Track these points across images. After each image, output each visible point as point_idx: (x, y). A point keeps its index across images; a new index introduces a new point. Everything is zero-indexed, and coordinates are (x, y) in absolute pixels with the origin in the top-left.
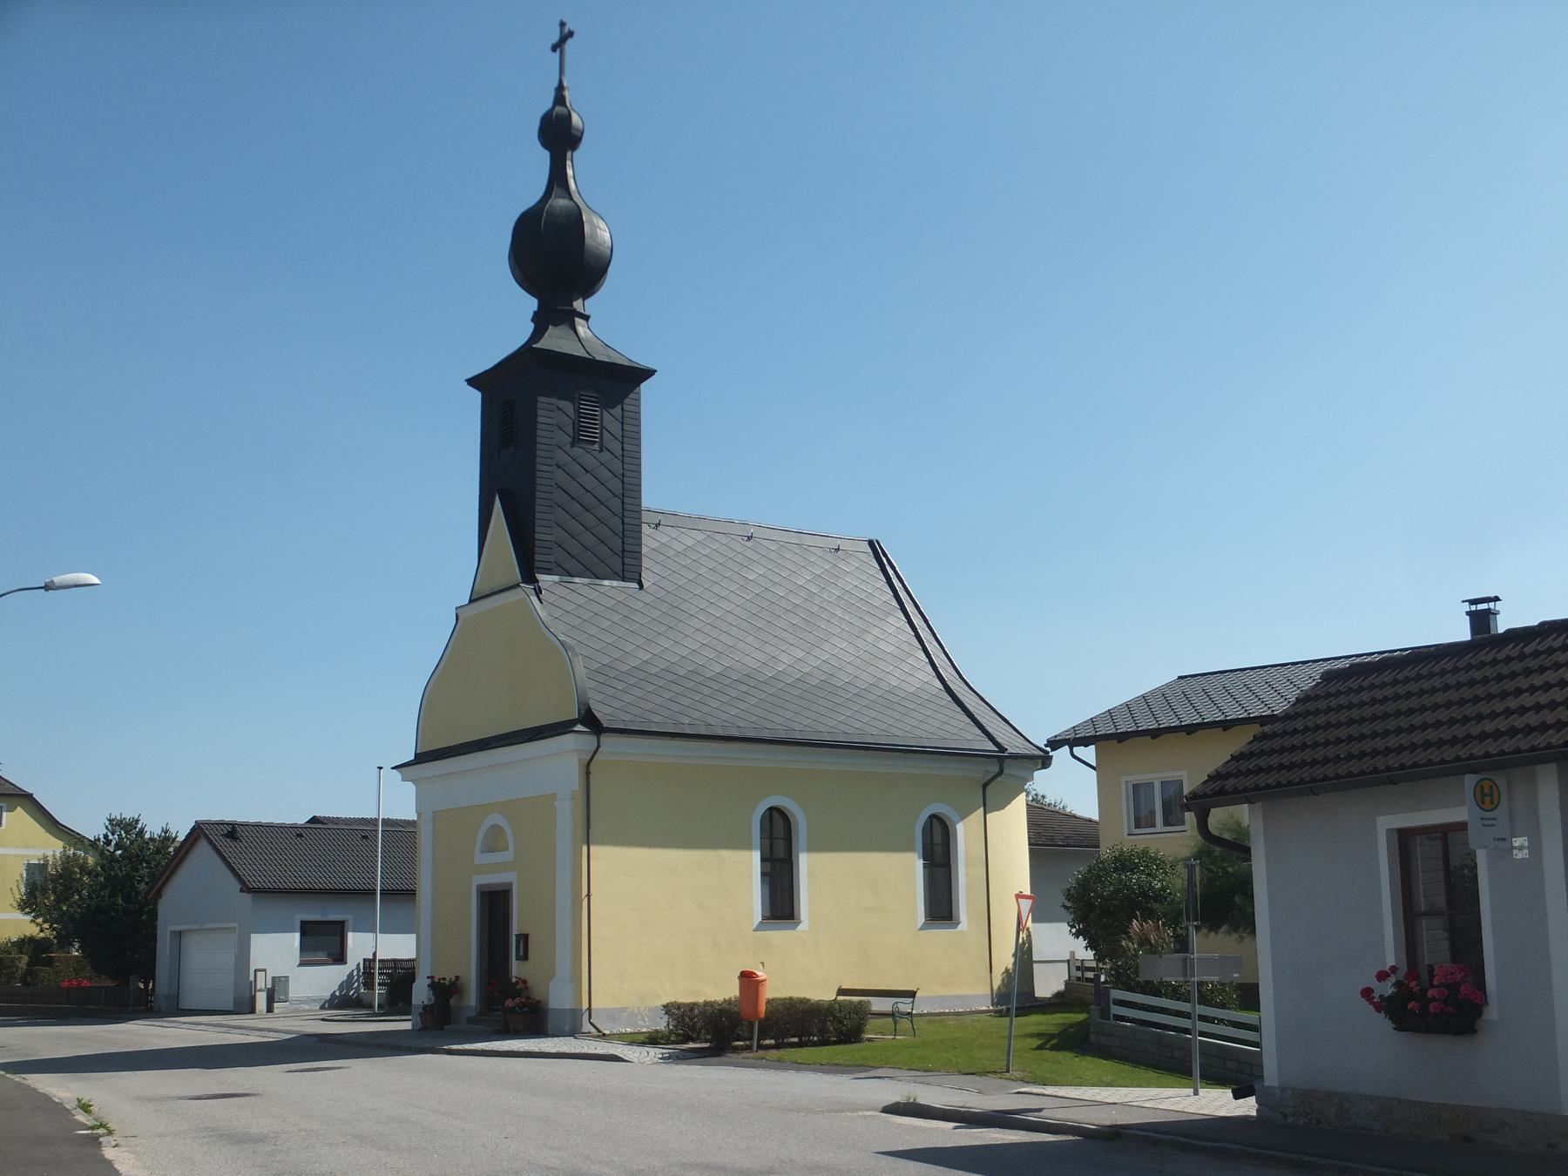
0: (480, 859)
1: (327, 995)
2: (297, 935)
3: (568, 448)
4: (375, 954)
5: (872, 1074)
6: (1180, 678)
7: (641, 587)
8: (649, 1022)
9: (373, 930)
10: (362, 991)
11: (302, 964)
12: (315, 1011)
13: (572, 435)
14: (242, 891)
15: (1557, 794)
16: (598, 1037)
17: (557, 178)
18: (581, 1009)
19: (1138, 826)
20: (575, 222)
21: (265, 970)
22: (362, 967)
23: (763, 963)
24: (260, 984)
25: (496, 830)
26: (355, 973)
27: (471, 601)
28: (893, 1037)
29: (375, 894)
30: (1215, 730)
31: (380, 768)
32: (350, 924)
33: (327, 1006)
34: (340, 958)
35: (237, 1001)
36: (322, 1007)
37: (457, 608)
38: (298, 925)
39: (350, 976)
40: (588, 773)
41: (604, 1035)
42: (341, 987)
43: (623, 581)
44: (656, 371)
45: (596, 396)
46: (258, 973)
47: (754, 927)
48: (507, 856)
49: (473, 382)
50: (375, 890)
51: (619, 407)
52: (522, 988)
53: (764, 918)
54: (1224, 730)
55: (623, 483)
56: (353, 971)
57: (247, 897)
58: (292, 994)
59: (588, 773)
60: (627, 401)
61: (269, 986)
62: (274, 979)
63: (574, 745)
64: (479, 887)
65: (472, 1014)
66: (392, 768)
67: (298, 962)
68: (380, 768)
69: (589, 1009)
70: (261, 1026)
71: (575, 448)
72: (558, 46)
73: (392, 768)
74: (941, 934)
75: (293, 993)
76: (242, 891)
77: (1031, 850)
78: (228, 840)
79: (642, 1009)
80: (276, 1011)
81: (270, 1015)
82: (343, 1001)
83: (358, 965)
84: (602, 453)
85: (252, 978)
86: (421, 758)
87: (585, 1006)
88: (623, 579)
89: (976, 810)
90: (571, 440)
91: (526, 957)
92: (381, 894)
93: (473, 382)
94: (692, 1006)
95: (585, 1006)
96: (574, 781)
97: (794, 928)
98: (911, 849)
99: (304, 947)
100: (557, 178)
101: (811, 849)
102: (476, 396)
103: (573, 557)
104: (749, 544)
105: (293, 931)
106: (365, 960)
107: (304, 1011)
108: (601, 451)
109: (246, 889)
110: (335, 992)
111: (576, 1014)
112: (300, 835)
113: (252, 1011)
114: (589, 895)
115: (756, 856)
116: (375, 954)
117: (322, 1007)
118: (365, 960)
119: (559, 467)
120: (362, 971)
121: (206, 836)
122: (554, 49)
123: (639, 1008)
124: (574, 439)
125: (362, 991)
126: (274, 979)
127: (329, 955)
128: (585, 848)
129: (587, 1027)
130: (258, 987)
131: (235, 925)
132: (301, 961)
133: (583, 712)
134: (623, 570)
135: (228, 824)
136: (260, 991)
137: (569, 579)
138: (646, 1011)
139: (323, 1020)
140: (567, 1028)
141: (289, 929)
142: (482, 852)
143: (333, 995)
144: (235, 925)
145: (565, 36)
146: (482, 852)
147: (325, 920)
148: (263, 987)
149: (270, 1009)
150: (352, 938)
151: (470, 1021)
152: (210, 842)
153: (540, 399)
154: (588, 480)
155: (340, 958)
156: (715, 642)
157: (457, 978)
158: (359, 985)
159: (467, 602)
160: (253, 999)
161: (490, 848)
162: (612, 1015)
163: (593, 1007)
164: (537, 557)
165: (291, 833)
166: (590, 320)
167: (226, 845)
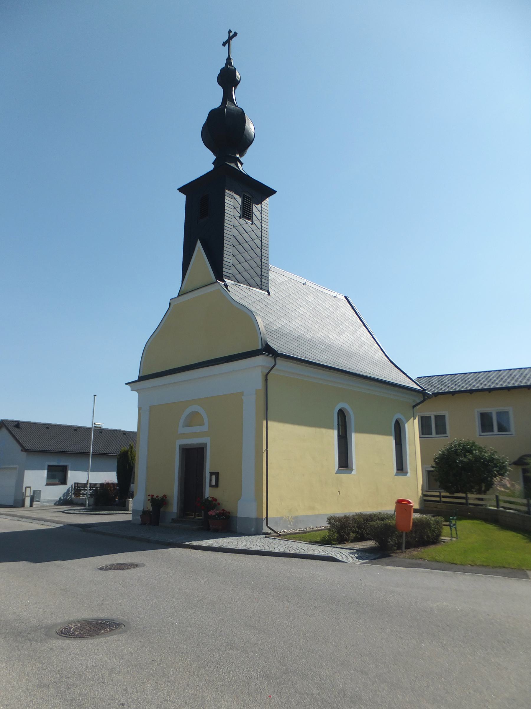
0: (182, 430)
1: (57, 499)
2: (46, 472)
3: (238, 218)
4: (88, 481)
5: (333, 546)
6: (418, 378)
7: (269, 294)
8: (293, 525)
9: (88, 471)
10: (73, 497)
11: (47, 484)
12: (51, 506)
13: (240, 213)
14: (22, 451)
15: (117, 465)
16: (277, 536)
17: (227, 97)
18: (263, 518)
19: (423, 434)
20: (240, 116)
21: (30, 487)
22: (73, 486)
23: (339, 491)
24: (28, 494)
25: (195, 414)
26: (70, 489)
27: (178, 296)
28: (450, 538)
29: (89, 454)
30: (449, 395)
31: (95, 395)
32: (69, 467)
33: (57, 504)
34: (64, 482)
35: (15, 501)
36: (55, 504)
37: (170, 299)
38: (46, 467)
39: (68, 490)
40: (266, 380)
41: (280, 535)
42: (64, 495)
43: (261, 290)
44: (276, 192)
45: (250, 197)
46: (27, 489)
47: (336, 472)
48: (205, 428)
49: (181, 190)
50: (89, 453)
51: (260, 205)
52: (213, 504)
53: (339, 467)
54: (453, 395)
55: (261, 242)
56: (69, 488)
57: (24, 454)
58: (42, 498)
59: (266, 380)
60: (263, 203)
61: (32, 494)
62: (34, 491)
63: (262, 361)
64: (180, 445)
65: (175, 516)
66: (126, 384)
67: (45, 484)
68: (95, 395)
69: (267, 518)
70: (35, 517)
71: (241, 219)
72: (226, 43)
73: (126, 384)
74: (401, 478)
75: (43, 497)
76: (22, 451)
77: (420, 440)
78: (16, 428)
79: (290, 518)
80: (34, 506)
81: (31, 509)
82: (64, 502)
83: (72, 485)
84: (253, 225)
85: (24, 491)
86: (141, 379)
87: (264, 516)
88: (261, 289)
89: (410, 419)
90: (240, 215)
91: (217, 485)
92: (92, 454)
93: (182, 190)
94: (346, 518)
95: (264, 516)
96: (260, 385)
97: (351, 473)
98: (391, 435)
99: (49, 477)
100: (227, 97)
101: (357, 431)
102: (183, 197)
103: (240, 273)
104: (304, 286)
105: (44, 470)
106: (75, 483)
107: (47, 506)
108: (252, 224)
109: (24, 449)
110: (61, 497)
111: (258, 521)
112: (48, 428)
113: (23, 506)
114: (267, 450)
115: (336, 432)
116: (88, 481)
117: (55, 504)
118: (75, 483)
119: (234, 227)
120: (74, 488)
121: (6, 426)
122: (224, 44)
123: (288, 517)
124: (241, 215)
125: (73, 497)
126: (34, 491)
127: (59, 481)
128: (265, 422)
129: (265, 530)
130: (27, 495)
131: (17, 466)
132: (47, 483)
133: (264, 345)
134: (261, 285)
135: (16, 421)
136: (27, 497)
137: (239, 284)
138: (292, 519)
139: (63, 512)
140: (253, 529)
141: (42, 469)
142: (183, 427)
143: (60, 499)
144: (17, 466)
145: (232, 36)
146: (183, 427)
147: (59, 465)
148: (29, 495)
149: (31, 505)
150: (70, 473)
151: (174, 521)
152: (8, 429)
153: (227, 191)
154: (245, 236)
155: (64, 482)
156: (304, 324)
157: (164, 496)
158: (72, 494)
159: (177, 296)
160: (23, 501)
161: (188, 424)
162: (278, 521)
163: (269, 517)
164: (224, 270)
165: (44, 427)
166: (243, 165)
167: (15, 431)
